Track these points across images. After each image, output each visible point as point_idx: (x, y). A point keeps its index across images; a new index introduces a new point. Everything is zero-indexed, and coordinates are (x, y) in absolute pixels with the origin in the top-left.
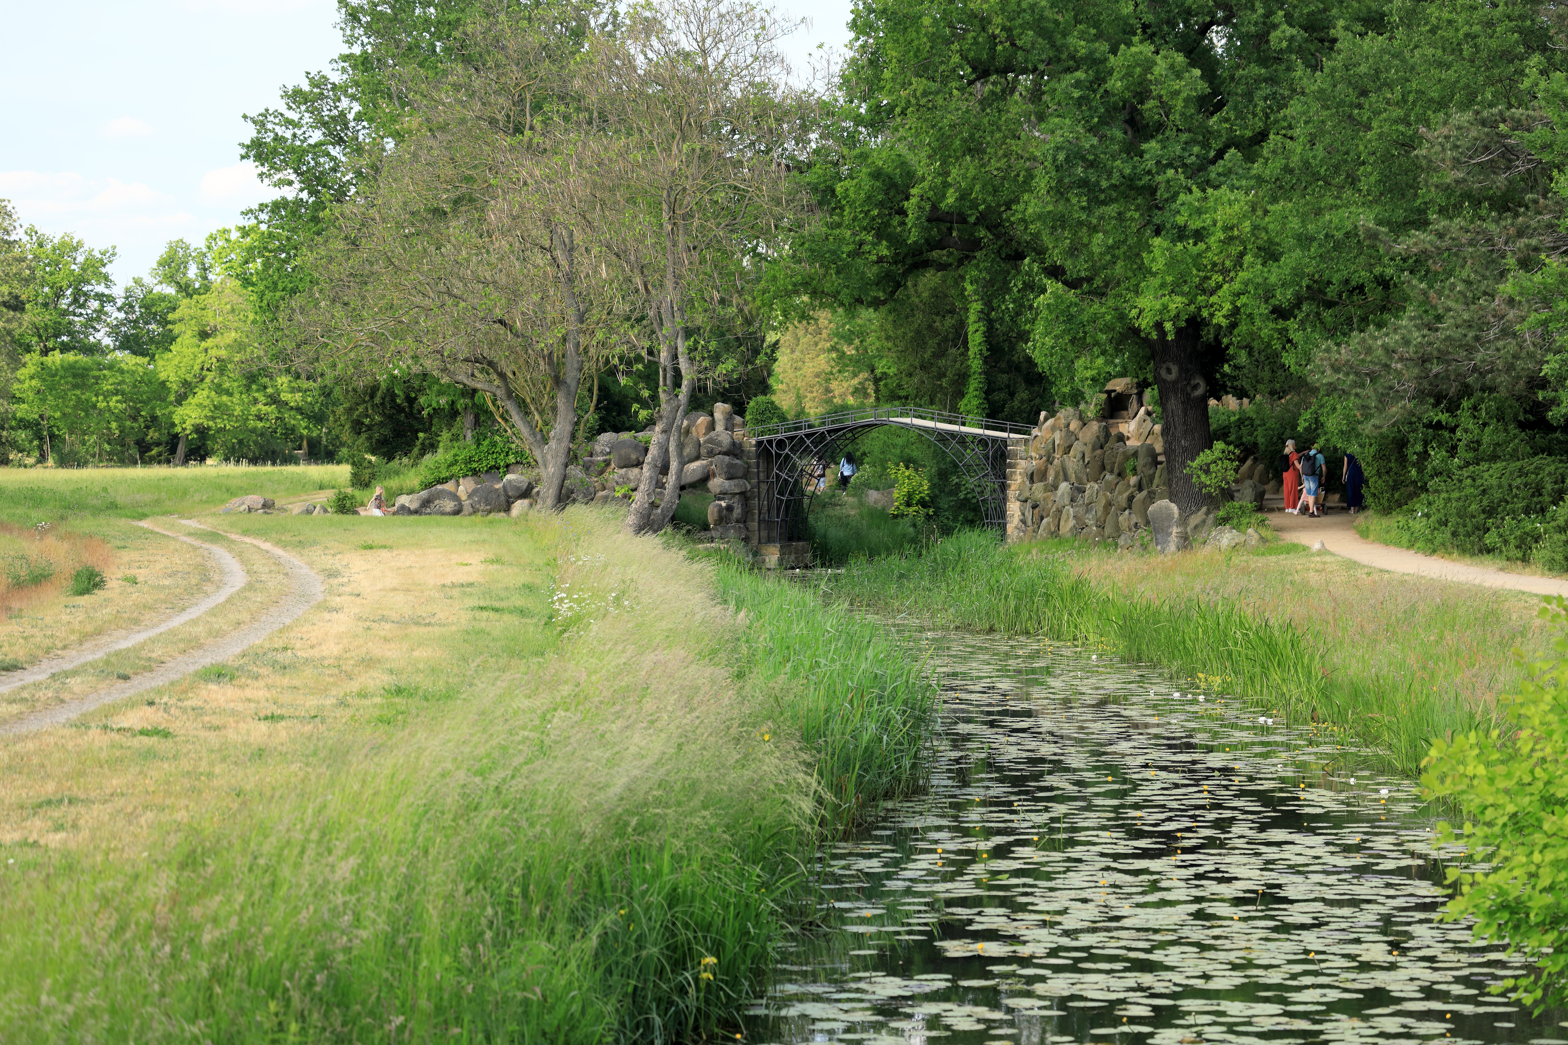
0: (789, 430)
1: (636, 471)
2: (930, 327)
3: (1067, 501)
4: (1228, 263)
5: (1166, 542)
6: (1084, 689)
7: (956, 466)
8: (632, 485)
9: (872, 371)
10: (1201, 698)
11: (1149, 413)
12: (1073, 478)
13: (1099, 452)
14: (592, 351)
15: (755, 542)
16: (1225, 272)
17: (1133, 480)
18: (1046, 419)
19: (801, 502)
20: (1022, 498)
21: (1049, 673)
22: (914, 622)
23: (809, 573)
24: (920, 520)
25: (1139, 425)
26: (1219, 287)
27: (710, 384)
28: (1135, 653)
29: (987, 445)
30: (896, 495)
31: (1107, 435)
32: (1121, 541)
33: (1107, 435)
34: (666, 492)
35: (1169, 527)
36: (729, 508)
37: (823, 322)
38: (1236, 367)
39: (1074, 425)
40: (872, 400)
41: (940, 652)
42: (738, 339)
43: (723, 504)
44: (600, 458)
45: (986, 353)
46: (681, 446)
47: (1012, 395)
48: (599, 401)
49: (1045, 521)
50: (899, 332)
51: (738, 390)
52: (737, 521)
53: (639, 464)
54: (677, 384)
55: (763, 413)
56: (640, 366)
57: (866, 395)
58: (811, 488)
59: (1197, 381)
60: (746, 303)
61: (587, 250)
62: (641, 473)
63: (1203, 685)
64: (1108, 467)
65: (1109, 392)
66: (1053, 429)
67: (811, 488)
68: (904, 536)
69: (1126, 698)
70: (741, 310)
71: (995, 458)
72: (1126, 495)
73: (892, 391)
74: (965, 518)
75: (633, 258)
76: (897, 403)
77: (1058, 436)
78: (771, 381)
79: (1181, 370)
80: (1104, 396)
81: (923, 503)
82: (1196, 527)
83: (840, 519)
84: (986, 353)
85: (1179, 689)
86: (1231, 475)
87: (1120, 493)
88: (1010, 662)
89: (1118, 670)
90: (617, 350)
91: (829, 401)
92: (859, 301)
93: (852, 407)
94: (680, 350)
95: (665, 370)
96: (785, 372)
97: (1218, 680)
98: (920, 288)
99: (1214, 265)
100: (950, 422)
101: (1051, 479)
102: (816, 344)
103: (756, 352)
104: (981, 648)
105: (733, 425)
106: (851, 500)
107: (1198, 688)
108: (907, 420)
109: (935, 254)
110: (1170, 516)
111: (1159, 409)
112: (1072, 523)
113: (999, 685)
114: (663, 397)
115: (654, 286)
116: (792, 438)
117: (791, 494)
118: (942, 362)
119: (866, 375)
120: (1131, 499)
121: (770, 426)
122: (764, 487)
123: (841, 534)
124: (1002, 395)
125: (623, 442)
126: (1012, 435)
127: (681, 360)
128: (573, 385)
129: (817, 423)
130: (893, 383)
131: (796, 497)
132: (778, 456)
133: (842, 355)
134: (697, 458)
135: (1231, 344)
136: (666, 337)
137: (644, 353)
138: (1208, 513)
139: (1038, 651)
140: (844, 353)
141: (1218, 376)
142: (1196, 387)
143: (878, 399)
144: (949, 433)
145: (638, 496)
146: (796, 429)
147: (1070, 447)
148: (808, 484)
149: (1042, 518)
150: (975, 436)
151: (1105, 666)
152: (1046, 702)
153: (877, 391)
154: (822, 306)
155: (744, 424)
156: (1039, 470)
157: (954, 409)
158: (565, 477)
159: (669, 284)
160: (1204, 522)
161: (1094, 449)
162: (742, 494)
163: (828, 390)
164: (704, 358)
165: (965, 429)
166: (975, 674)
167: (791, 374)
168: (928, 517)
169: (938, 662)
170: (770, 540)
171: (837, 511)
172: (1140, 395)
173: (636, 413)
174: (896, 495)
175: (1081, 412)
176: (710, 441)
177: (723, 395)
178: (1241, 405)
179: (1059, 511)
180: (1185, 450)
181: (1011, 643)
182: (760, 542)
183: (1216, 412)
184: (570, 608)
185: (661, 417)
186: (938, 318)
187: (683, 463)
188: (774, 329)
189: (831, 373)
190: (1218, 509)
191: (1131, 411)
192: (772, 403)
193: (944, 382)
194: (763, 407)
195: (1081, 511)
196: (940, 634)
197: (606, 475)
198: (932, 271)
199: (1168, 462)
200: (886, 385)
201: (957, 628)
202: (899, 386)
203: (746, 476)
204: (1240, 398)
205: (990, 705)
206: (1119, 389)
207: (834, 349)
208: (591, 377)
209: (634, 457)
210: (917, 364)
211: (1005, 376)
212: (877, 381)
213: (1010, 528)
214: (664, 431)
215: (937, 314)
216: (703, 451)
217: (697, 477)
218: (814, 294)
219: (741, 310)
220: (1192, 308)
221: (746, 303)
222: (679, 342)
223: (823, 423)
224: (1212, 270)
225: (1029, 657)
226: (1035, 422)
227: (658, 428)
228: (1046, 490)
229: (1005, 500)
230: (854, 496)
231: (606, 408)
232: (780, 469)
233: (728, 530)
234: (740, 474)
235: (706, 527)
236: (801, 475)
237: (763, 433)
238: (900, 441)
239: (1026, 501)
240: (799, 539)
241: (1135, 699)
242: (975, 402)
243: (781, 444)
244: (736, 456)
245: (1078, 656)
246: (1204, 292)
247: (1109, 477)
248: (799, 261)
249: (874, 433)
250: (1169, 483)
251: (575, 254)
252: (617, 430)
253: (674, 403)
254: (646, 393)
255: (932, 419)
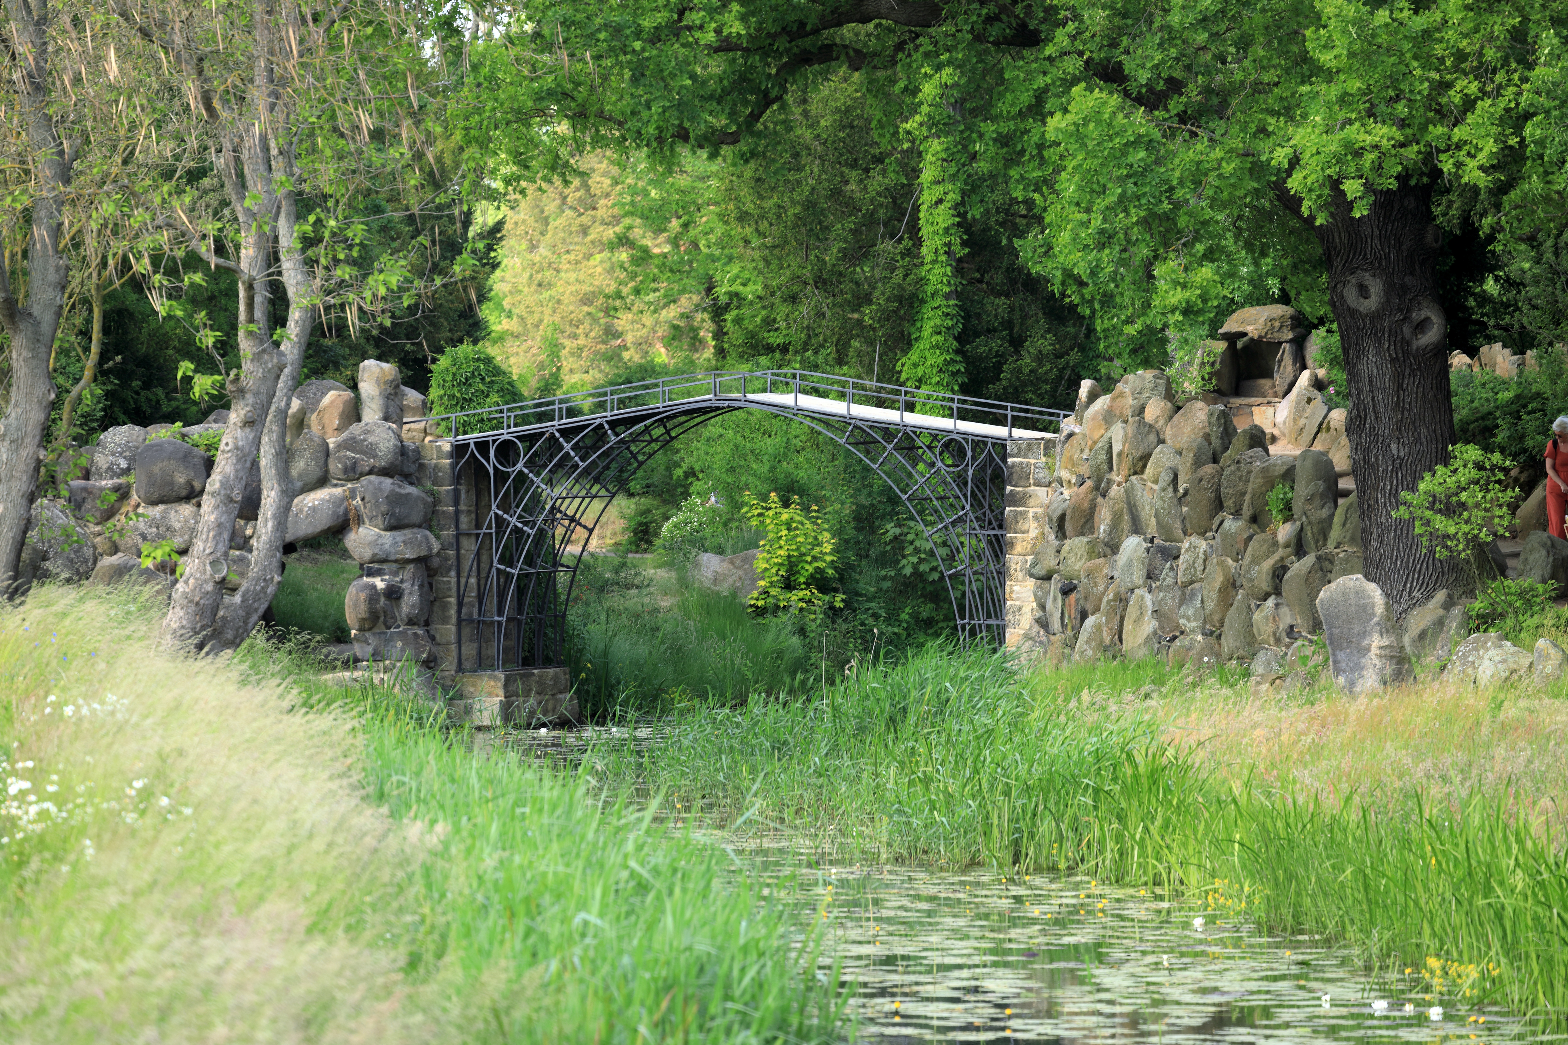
0: (525, 420)
1: (186, 510)
2: (836, 193)
3: (1138, 577)
4: (1490, 54)
5: (1359, 668)
6: (1175, 993)
7: (894, 500)
8: (178, 542)
9: (709, 290)
10: (1435, 1013)
11: (1319, 385)
12: (1152, 528)
13: (1209, 469)
14: (91, 244)
15: (448, 666)
16: (1483, 72)
17: (1285, 531)
18: (1093, 397)
19: (551, 580)
20: (1039, 571)
21: (1101, 959)
22: (804, 845)
23: (570, 738)
24: (815, 620)
25: (1298, 412)
26: (1469, 104)
27: (352, 317)
28: (1287, 914)
29: (962, 453)
30: (761, 565)
31: (1228, 432)
32: (1258, 666)
33: (1228, 432)
34: (253, 557)
35: (1364, 634)
36: (393, 594)
37: (600, 182)
38: (1510, 283)
39: (1155, 410)
40: (708, 353)
41: (859, 912)
42: (411, 219)
43: (380, 584)
44: (107, 483)
45: (961, 252)
46: (285, 456)
47: (1017, 343)
48: (104, 357)
49: (1090, 621)
50: (769, 204)
51: (412, 332)
52: (411, 622)
53: (192, 495)
54: (278, 319)
55: (467, 383)
56: (198, 278)
57: (696, 343)
58: (574, 549)
59: (1425, 313)
60: (430, 139)
61: (77, 22)
62: (197, 516)
63: (1437, 983)
64: (1229, 503)
65: (1232, 338)
66: (1109, 418)
67: (574, 549)
68: (780, 654)
69: (1266, 1012)
70: (419, 156)
71: (979, 482)
72: (1268, 564)
73: (753, 335)
74: (915, 616)
75: (179, 40)
76: (763, 360)
77: (1118, 434)
78: (486, 312)
79: (1390, 289)
80: (1221, 346)
81: (821, 583)
82: (1422, 635)
83: (637, 616)
84: (961, 252)
85: (1385, 992)
86: (1502, 520)
87: (1256, 560)
88: (1014, 933)
89: (1253, 952)
90: (145, 243)
91: (613, 357)
92: (683, 136)
93: (665, 370)
94: (284, 242)
95: (250, 287)
96: (515, 291)
97: (1472, 972)
98: (814, 108)
99: (1461, 56)
100: (880, 404)
101: (1103, 528)
102: (584, 231)
103: (452, 248)
104: (949, 902)
105: (402, 410)
106: (663, 574)
107: (1427, 989)
108: (786, 399)
109: (848, 32)
110: (1365, 611)
111: (1341, 376)
112: (1149, 625)
113: (988, 984)
114: (245, 345)
115: (225, 102)
116: (530, 439)
117: (530, 561)
118: (863, 271)
119: (696, 298)
120: (1279, 573)
121: (484, 411)
122: (469, 546)
123: (643, 650)
124: (996, 344)
125: (158, 447)
126: (1018, 433)
127: (287, 265)
128: (46, 319)
129: (586, 404)
130: (754, 318)
131: (541, 567)
132: (501, 477)
133: (643, 257)
134: (322, 481)
135: (1497, 228)
136: (253, 215)
137: (205, 250)
138: (1448, 605)
139: (1075, 910)
140: (646, 250)
141: (1472, 303)
142: (1422, 326)
143: (721, 352)
144: (875, 425)
145: (189, 566)
146: (541, 417)
147: (1145, 458)
148: (566, 540)
149: (1084, 616)
150: (935, 434)
151: (1222, 942)
152: (1092, 1020)
153: (719, 334)
154: (598, 141)
155: (426, 408)
156: (1076, 509)
157: (889, 374)
158: (28, 524)
159: (258, 95)
160: (1440, 623)
161: (1198, 463)
162: (422, 561)
163: (611, 333)
164: (337, 261)
165: (913, 419)
166: (936, 958)
167: (529, 296)
168: (833, 612)
169: (854, 934)
170: (482, 664)
171: (633, 600)
172: (1299, 344)
173: (188, 380)
174: (761, 565)
175: (1168, 380)
176: (351, 444)
177: (378, 342)
178: (1521, 365)
179: (1122, 600)
180: (1399, 464)
181: (1015, 890)
182: (460, 669)
183: (1468, 381)
184: (43, 815)
185: (242, 392)
186: (854, 175)
187: (289, 494)
188: (492, 196)
189: (619, 295)
190: (1471, 594)
191: (1280, 380)
192: (488, 360)
193: (867, 314)
194: (467, 370)
195: (1170, 599)
196: (857, 871)
197: (119, 520)
198: (843, 70)
199: (1362, 490)
200: (738, 321)
201: (898, 859)
202: (769, 323)
203: (429, 522)
204: (1521, 352)
205: (969, 1027)
206: (1252, 330)
207: (624, 241)
208: (86, 301)
209: (181, 479)
210: (807, 273)
211: (1002, 302)
212: (718, 312)
213: (1013, 636)
214: (248, 423)
215: (854, 165)
216: (335, 467)
217: (322, 523)
218: (579, 117)
219: (419, 156)
220: (1412, 152)
221: (430, 139)
222: (283, 225)
223: (601, 406)
224: (1456, 68)
225: (1057, 922)
226: (1069, 404)
227: (235, 416)
228: (1093, 552)
229: (1002, 574)
230: (669, 565)
231: (121, 372)
232: (505, 506)
233: (388, 641)
234: (416, 517)
235: (340, 636)
236: (551, 520)
237: (466, 427)
238: (769, 445)
239: (1048, 578)
240: (548, 662)
241: (1286, 1015)
242: (937, 359)
243: (506, 450)
244: (407, 477)
245: (1165, 920)
246: (1441, 113)
247: (1231, 524)
248: (548, 47)
249: (714, 428)
250: (1363, 538)
251: (52, 32)
252: (143, 419)
253: (272, 361)
254: (208, 339)
255: (842, 396)
